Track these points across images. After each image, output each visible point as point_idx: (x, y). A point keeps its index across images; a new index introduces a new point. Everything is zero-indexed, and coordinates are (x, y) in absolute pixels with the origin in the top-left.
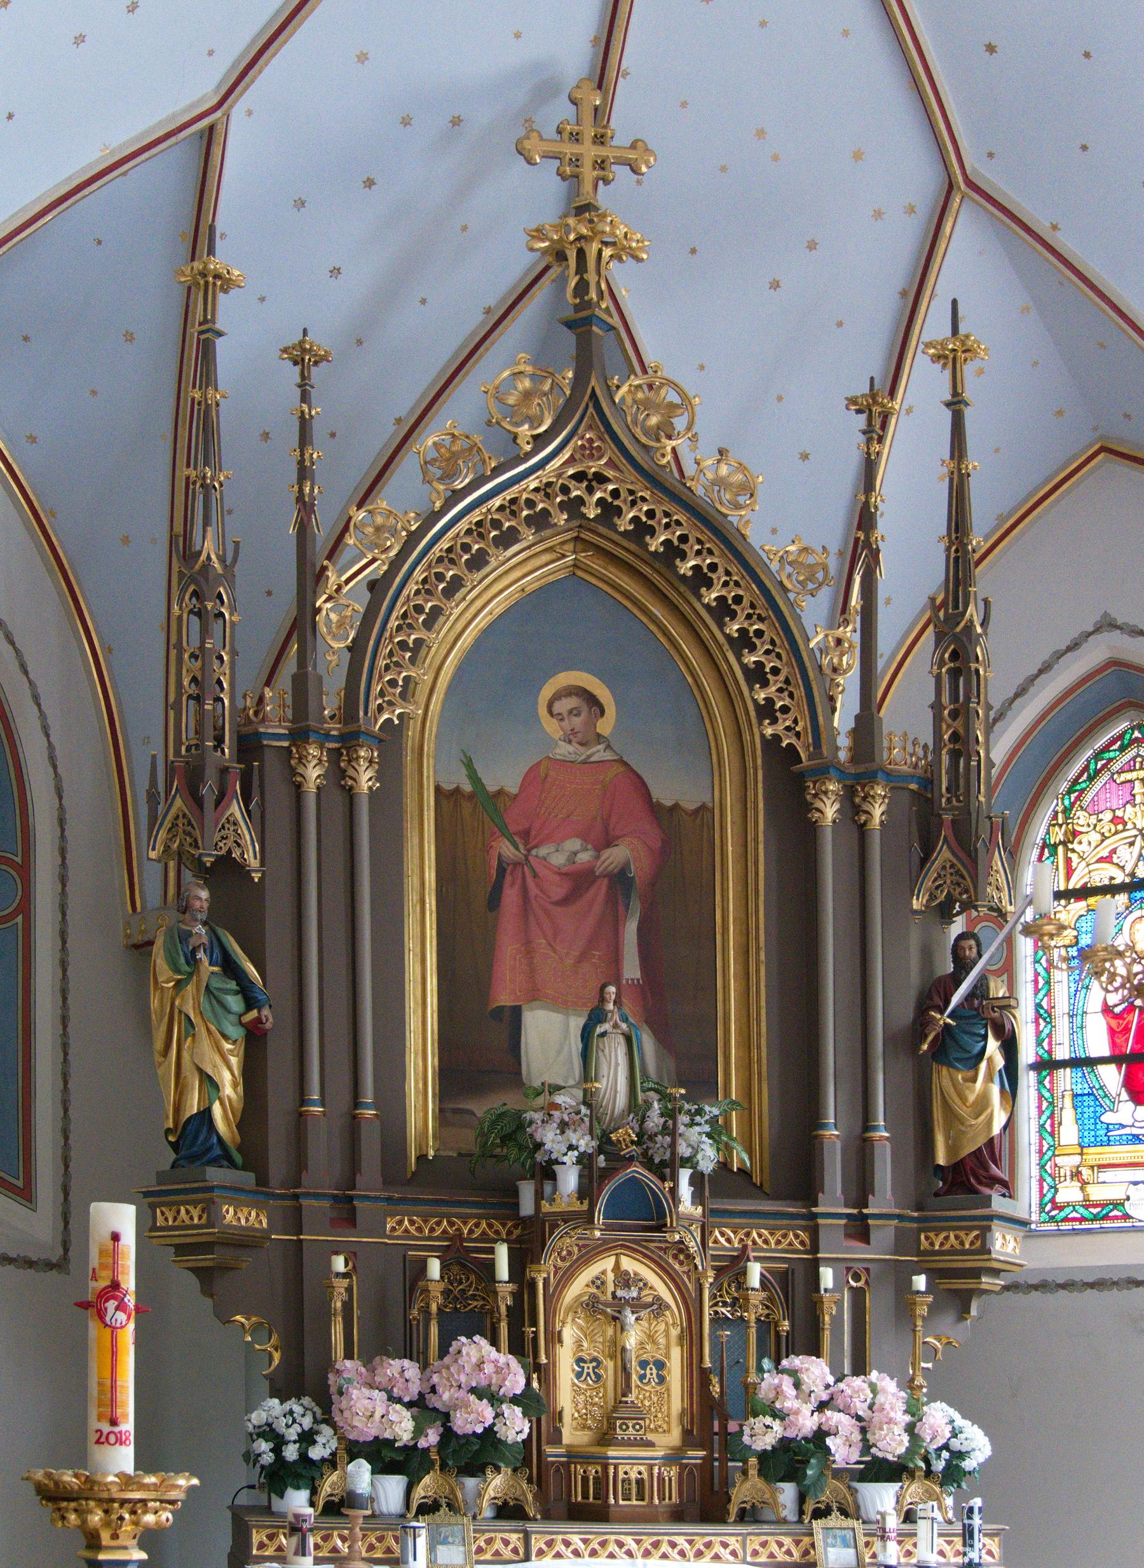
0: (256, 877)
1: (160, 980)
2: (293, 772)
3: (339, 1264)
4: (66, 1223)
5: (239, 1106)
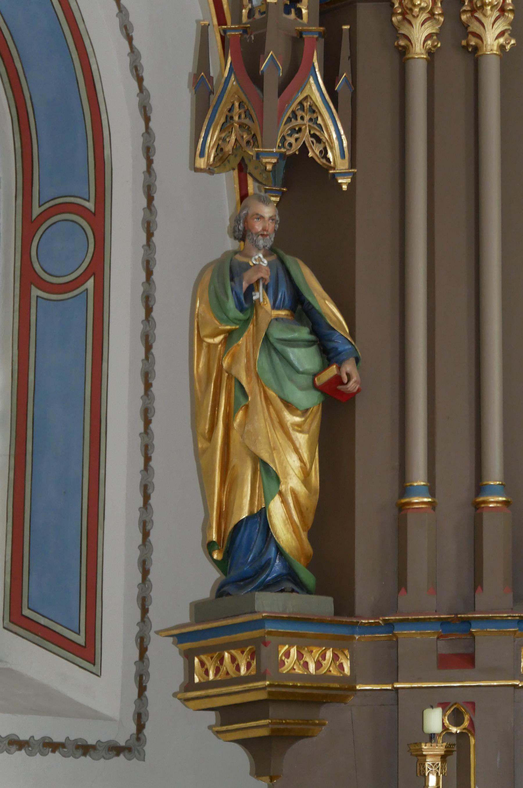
0: (344, 182)
1: (202, 334)
2: (395, 32)
3: (434, 720)
4: (142, 689)
5: (310, 502)
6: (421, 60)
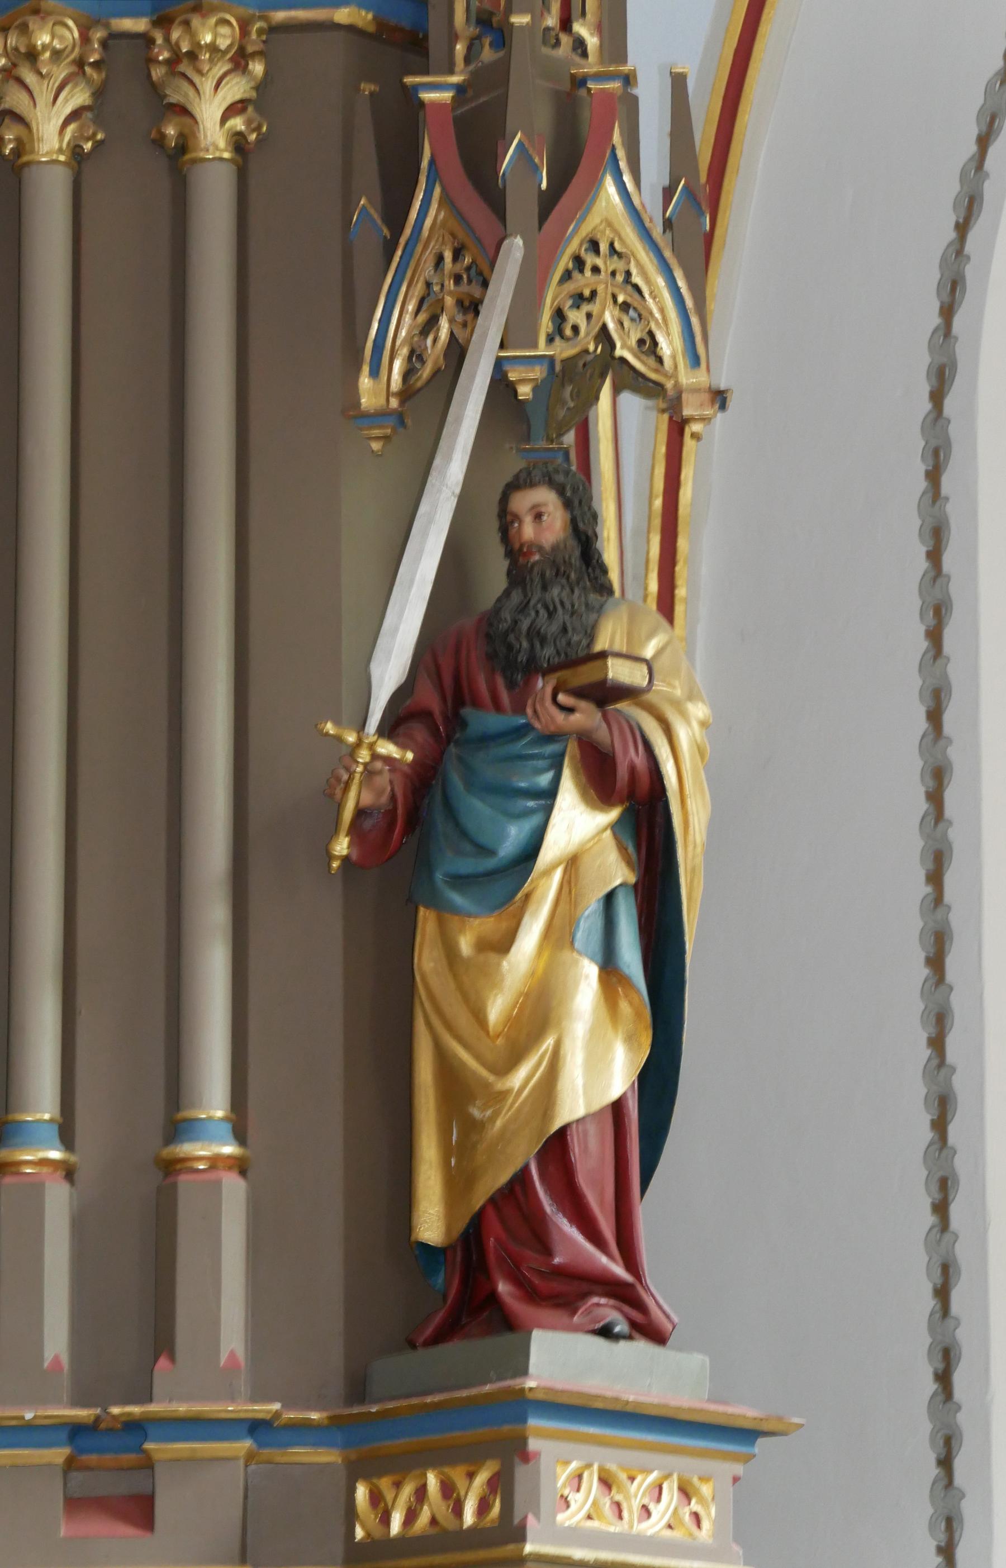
6: (217, 165)
